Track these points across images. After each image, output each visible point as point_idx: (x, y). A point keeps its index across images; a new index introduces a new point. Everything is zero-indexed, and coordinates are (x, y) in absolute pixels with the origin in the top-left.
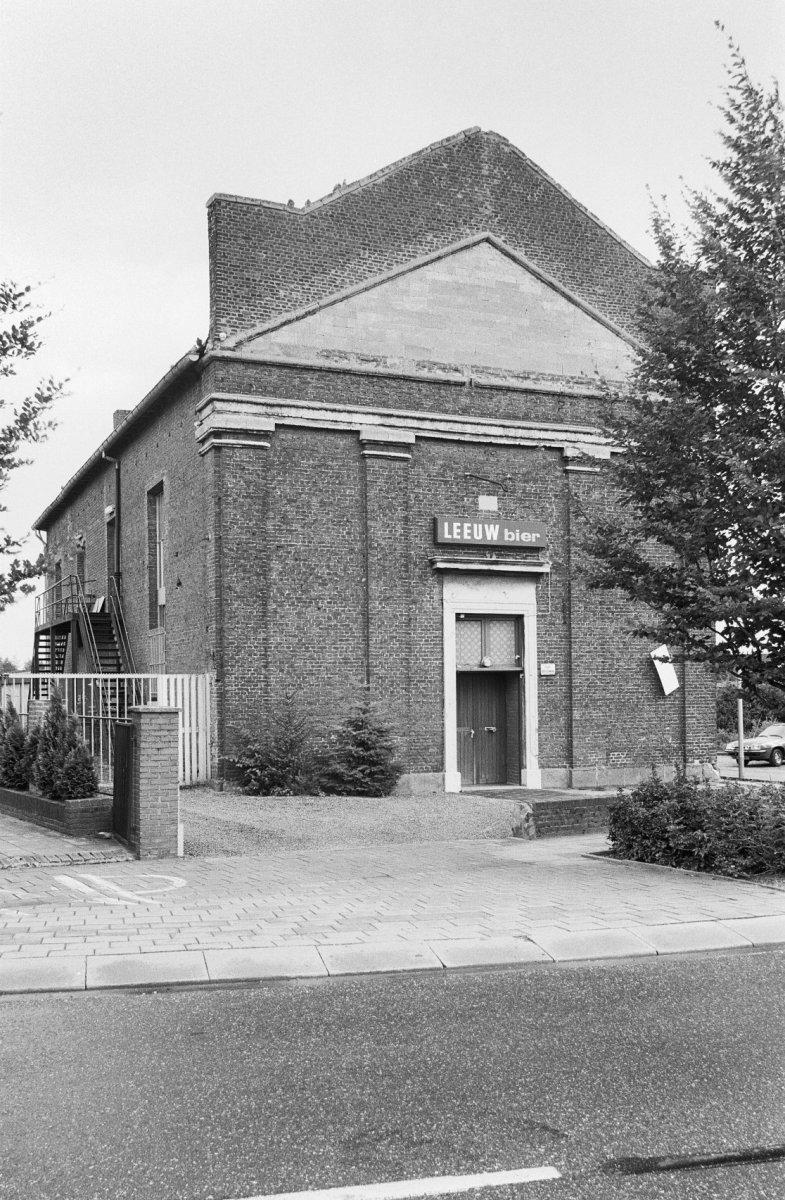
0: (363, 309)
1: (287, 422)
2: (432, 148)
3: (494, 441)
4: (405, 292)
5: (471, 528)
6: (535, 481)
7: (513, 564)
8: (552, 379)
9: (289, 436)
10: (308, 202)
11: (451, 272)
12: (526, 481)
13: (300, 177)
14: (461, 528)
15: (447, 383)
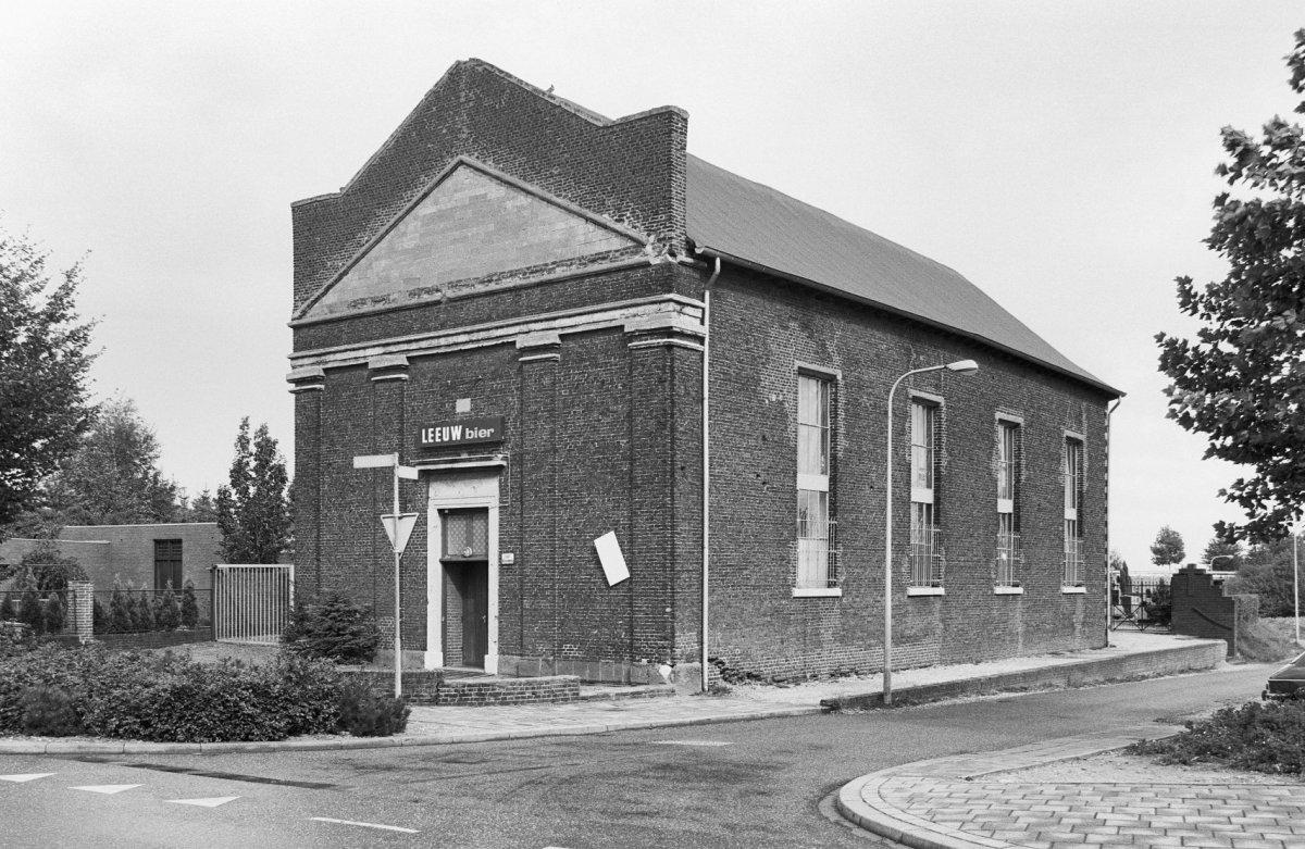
0: (377, 259)
1: (329, 366)
2: (428, 96)
3: (485, 344)
4: (404, 234)
5: (441, 432)
6: (501, 377)
7: (470, 460)
8: (511, 276)
9: (337, 376)
10: (551, 89)
11: (436, 203)
12: (494, 379)
13: (334, 175)
14: (433, 432)
15: (427, 305)
